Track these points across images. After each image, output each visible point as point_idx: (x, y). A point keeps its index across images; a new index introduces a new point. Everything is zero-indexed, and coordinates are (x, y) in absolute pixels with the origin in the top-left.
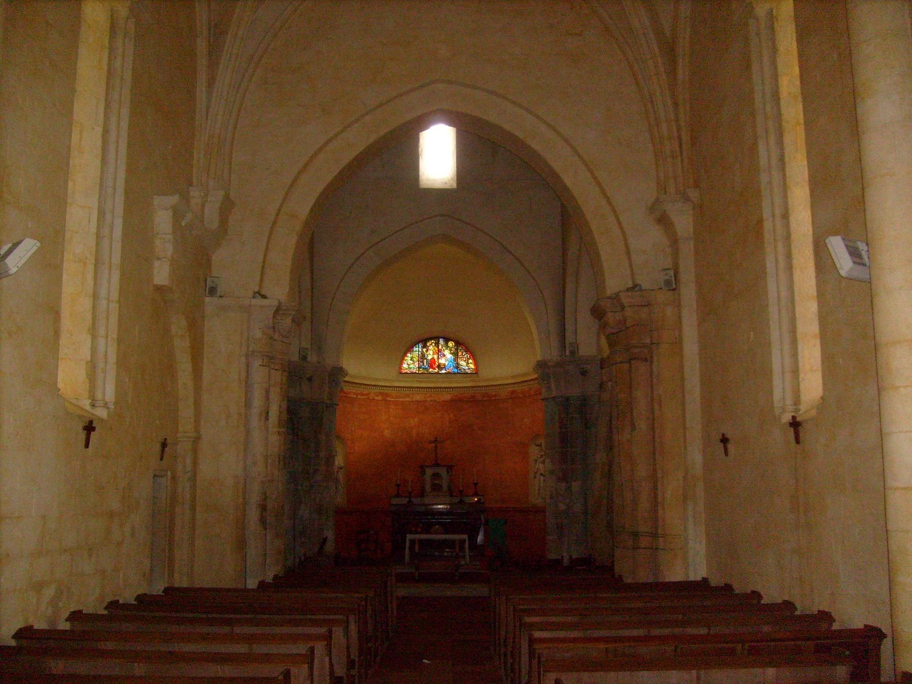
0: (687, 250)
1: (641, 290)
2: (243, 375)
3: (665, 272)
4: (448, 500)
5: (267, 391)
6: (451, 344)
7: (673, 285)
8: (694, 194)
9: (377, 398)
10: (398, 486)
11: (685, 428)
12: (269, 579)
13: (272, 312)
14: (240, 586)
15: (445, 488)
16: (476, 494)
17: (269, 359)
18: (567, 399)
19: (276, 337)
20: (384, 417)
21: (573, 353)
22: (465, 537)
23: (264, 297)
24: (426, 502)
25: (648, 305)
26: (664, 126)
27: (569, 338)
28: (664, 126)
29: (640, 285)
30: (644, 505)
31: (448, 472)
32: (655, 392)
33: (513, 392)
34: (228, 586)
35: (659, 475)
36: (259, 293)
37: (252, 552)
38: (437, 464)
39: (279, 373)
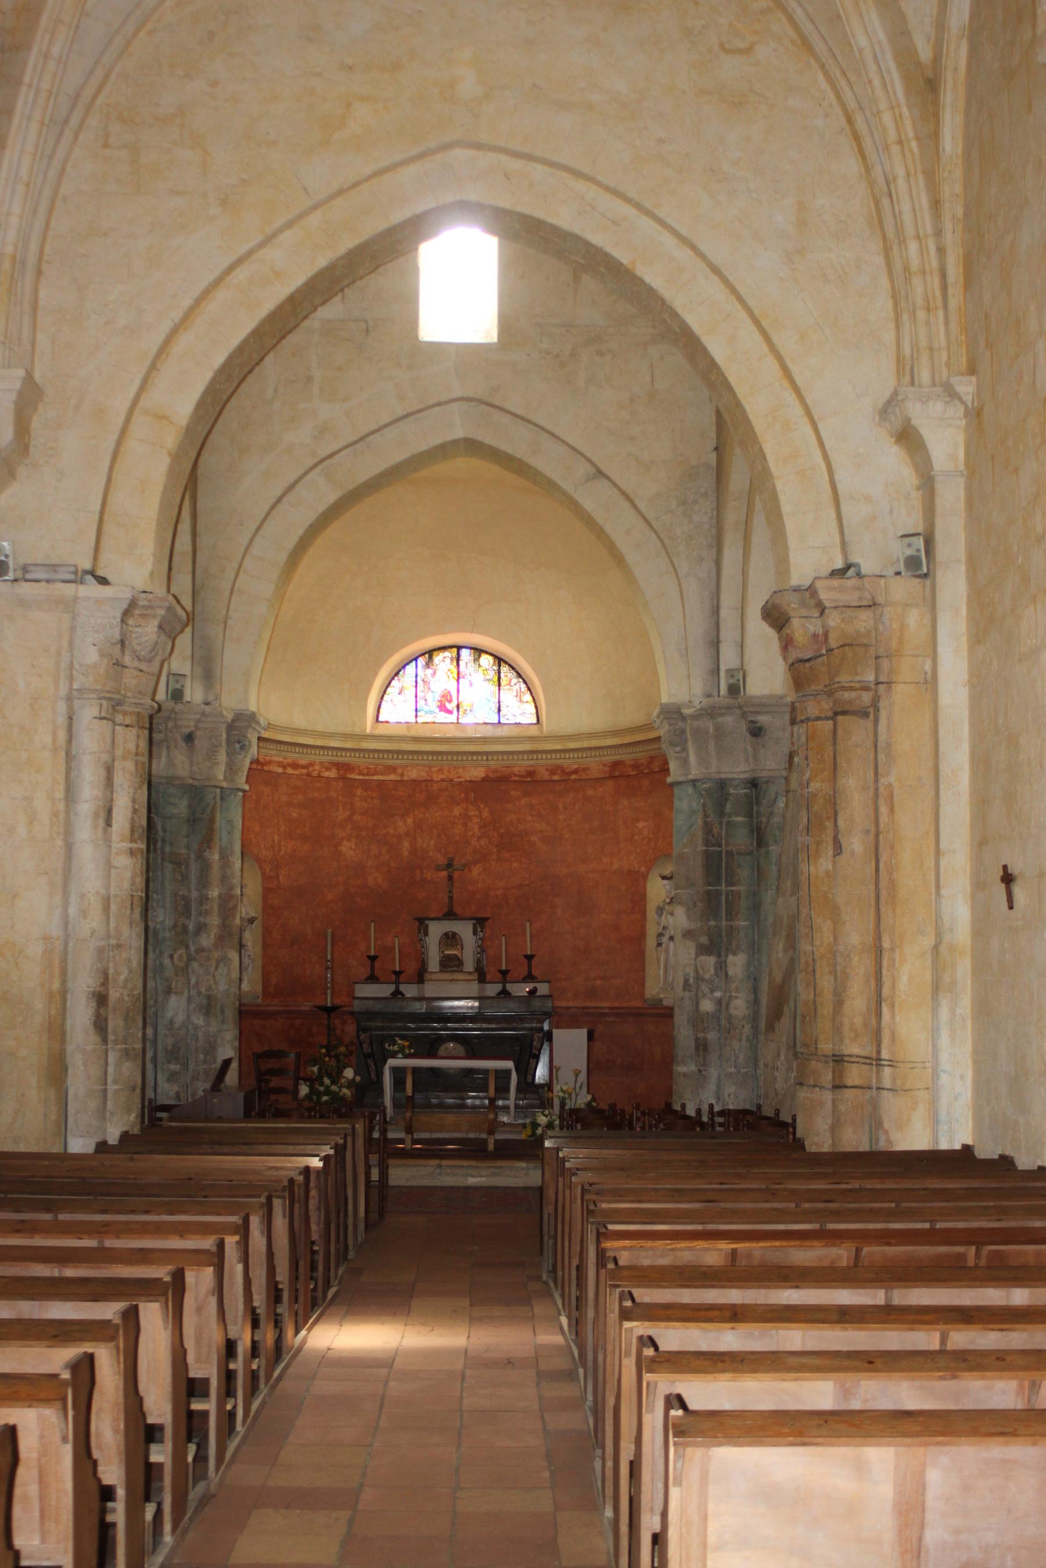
0: (951, 495)
1: (859, 575)
2: (62, 735)
3: (907, 540)
4: (474, 988)
5: (109, 770)
6: (486, 660)
7: (920, 566)
8: (966, 387)
9: (326, 774)
10: (373, 959)
11: (938, 853)
12: (113, 1136)
13: (118, 615)
14: (57, 1149)
15: (469, 965)
16: (530, 978)
17: (113, 707)
18: (722, 785)
19: (127, 660)
20: (341, 815)
21: (734, 690)
22: (509, 1064)
23: (103, 581)
24: (428, 995)
25: (873, 605)
26: (913, 247)
27: (728, 659)
28: (913, 247)
29: (856, 565)
30: (857, 1003)
31: (475, 933)
32: (882, 781)
33: (615, 765)
34: (34, 1149)
35: (886, 944)
36: (92, 573)
37: (80, 1080)
38: (450, 915)
39: (134, 731)
